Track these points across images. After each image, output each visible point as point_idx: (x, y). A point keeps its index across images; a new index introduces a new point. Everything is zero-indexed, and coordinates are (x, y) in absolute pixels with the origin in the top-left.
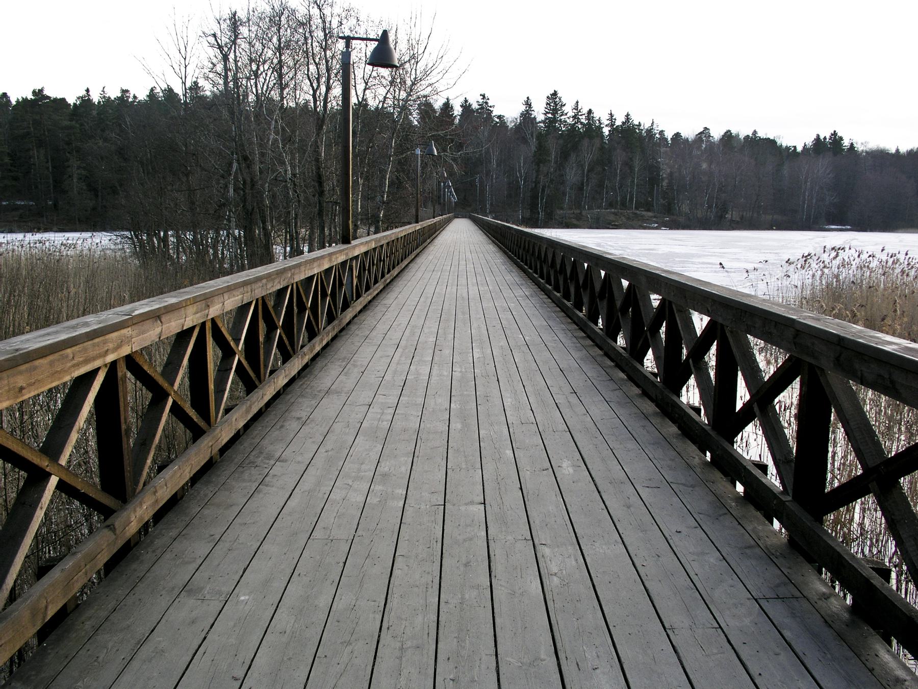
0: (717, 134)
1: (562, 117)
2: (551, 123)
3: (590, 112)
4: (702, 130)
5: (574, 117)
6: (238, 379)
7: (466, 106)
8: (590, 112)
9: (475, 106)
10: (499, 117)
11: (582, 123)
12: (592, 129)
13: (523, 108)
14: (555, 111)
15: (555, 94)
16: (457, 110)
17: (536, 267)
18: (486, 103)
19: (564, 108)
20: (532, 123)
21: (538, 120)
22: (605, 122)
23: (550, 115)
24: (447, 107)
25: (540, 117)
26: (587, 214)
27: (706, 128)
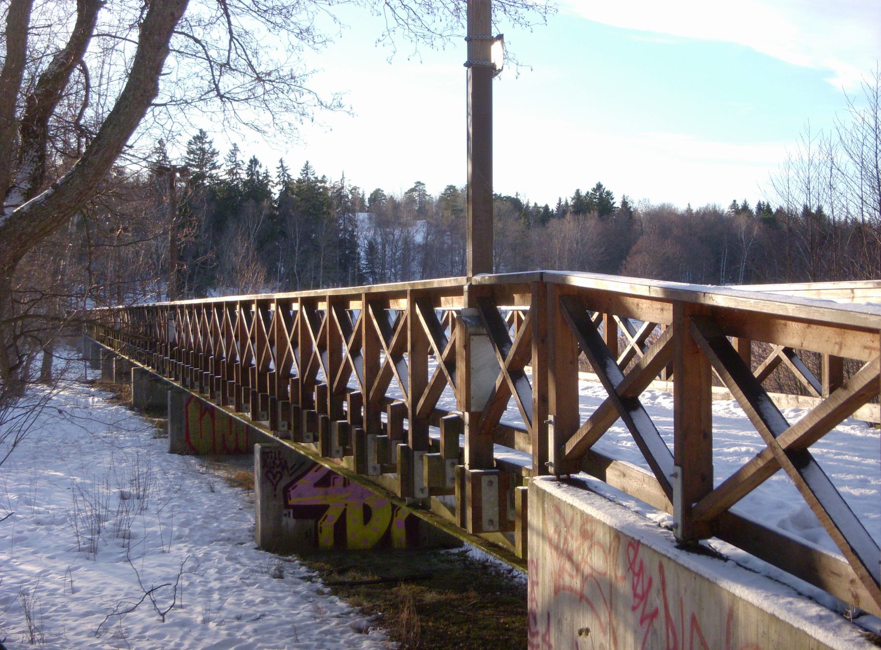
1: (214, 172)
3: (254, 162)
4: (413, 186)
5: (231, 172)
8: (254, 162)
12: (257, 188)
19: (215, 159)
27: (419, 183)
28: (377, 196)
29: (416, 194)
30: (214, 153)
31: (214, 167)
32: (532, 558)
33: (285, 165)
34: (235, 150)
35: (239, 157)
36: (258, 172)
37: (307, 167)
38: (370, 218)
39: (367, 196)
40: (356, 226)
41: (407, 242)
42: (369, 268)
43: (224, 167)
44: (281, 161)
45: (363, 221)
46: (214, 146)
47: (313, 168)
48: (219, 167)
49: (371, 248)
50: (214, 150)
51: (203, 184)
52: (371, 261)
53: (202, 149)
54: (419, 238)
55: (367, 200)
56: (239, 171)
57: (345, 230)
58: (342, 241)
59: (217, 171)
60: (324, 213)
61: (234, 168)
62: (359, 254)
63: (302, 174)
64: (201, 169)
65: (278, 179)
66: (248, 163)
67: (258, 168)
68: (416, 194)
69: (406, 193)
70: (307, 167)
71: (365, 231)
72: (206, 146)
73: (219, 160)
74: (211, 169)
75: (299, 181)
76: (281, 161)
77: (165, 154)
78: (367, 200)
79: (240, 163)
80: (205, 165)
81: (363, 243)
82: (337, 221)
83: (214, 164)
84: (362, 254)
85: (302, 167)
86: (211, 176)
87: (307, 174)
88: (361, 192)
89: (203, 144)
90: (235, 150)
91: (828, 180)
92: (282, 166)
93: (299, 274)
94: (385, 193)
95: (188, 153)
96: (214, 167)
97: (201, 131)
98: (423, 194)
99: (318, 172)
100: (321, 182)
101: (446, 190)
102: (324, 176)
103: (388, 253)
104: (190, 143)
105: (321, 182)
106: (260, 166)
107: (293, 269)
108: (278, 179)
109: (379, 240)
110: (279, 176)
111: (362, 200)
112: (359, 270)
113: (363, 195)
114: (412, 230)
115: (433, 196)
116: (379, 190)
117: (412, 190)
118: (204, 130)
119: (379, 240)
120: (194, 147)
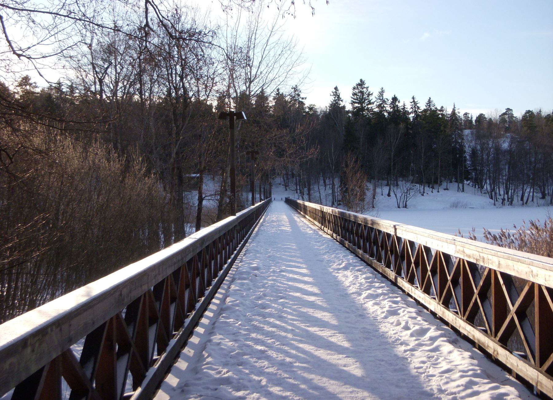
0: (518, 114)
1: (369, 106)
2: (358, 112)
3: (395, 99)
4: (504, 111)
5: (379, 106)
6: (126, 391)
7: (280, 98)
8: (395, 99)
9: (288, 98)
10: (311, 109)
11: (386, 111)
12: (398, 115)
13: (332, 98)
14: (361, 101)
15: (361, 84)
16: (272, 103)
17: (373, 251)
18: (299, 95)
19: (371, 98)
20: (341, 112)
21: (347, 109)
22: (409, 108)
23: (356, 105)
24: (262, 97)
25: (349, 107)
26: (180, 257)
27: (508, 109)
28: (481, 118)
29: (506, 116)
30: (369, 95)
31: (370, 103)
32: (547, 391)
33: (416, 100)
34: (382, 93)
35: (385, 96)
36: (397, 106)
37: (430, 102)
38: (472, 134)
39: (474, 119)
40: (463, 139)
41: (498, 149)
42: (473, 166)
43: (375, 103)
44: (413, 98)
45: (467, 136)
46: (369, 90)
47: (434, 102)
48: (373, 103)
49: (474, 153)
50: (369, 92)
51: (363, 114)
52: (474, 164)
53: (362, 92)
54: (505, 145)
55: (474, 121)
56: (385, 105)
57: (456, 142)
58: (454, 149)
59: (372, 105)
60: (442, 131)
61: (382, 104)
62: (465, 157)
63: (426, 106)
64: (362, 105)
65: (411, 110)
66: (390, 100)
67: (397, 103)
68: (506, 116)
69: (500, 116)
70: (430, 102)
71: (469, 141)
72: (365, 90)
73: (373, 98)
74: (368, 105)
75: (425, 111)
76: (413, 98)
77: (339, 96)
78: (474, 121)
79: (386, 100)
80: (364, 102)
81: (468, 150)
82: (450, 136)
83: (369, 101)
84: (468, 157)
85: (426, 101)
86: (368, 109)
87: (430, 106)
88: (470, 116)
89: (362, 88)
90: (382, 93)
91: (229, 16)
92: (414, 101)
93: (424, 172)
94: (486, 116)
95: (353, 95)
96: (370, 103)
97: (361, 80)
98: (512, 116)
99: (438, 105)
100: (440, 111)
101: (526, 113)
102: (442, 107)
103: (485, 157)
104: (354, 88)
105: (440, 111)
106: (399, 102)
107: (420, 168)
108: (411, 110)
109: (479, 147)
110: (412, 108)
111: (471, 121)
112: (465, 167)
113: (472, 118)
114: (501, 141)
115: (518, 117)
116: (482, 114)
117: (504, 114)
118: (363, 80)
119: (479, 147)
120: (357, 91)
